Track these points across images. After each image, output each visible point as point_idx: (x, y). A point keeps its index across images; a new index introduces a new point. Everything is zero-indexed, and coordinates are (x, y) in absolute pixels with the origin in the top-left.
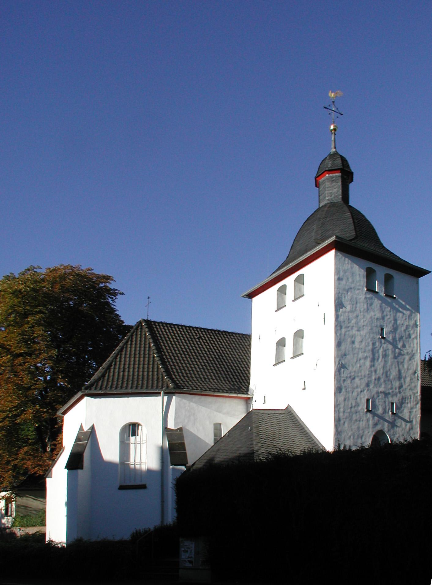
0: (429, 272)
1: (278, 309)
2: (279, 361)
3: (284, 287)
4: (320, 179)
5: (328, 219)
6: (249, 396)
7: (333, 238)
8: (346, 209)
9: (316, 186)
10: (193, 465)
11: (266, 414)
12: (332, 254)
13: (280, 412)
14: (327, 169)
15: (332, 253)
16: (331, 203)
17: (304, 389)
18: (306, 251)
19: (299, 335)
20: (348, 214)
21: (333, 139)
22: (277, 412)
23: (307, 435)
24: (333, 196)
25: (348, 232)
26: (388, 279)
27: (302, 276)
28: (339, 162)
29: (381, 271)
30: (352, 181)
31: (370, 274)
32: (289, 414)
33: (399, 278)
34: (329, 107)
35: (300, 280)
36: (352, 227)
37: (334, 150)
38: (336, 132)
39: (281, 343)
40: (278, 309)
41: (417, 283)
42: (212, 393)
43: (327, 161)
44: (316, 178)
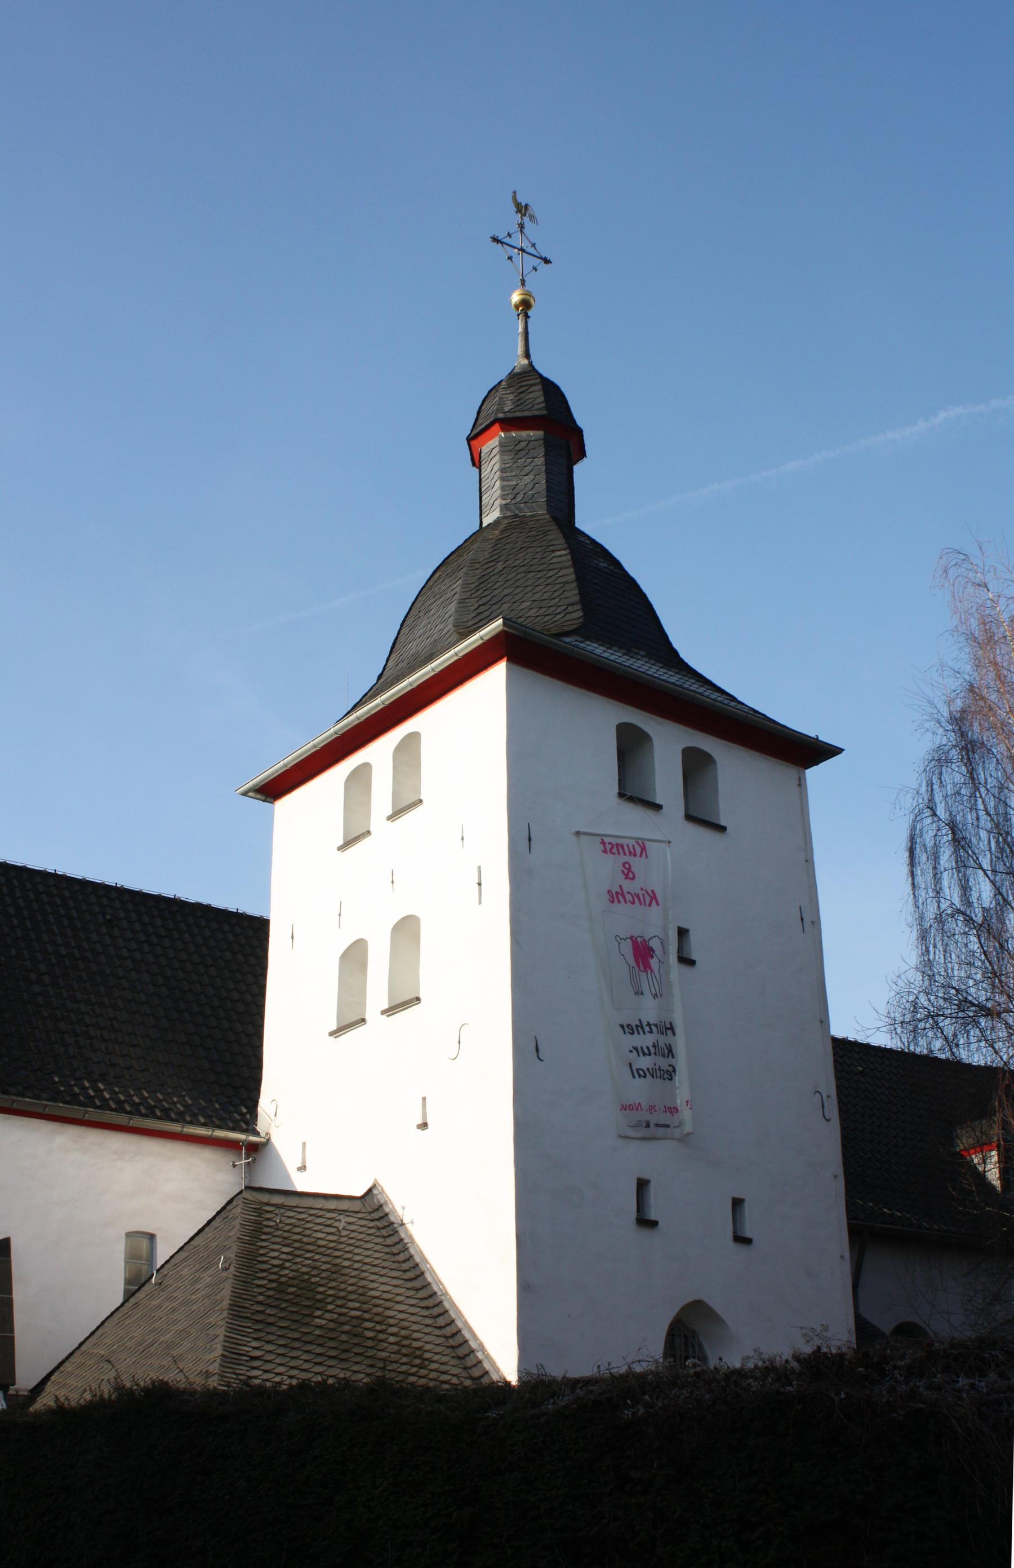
0: (245, 794)
1: (348, 844)
2: (348, 1023)
3: (363, 772)
4: (484, 444)
5: (500, 566)
6: (253, 1139)
7: (496, 625)
8: (556, 537)
9: (474, 464)
10: (39, 1388)
11: (290, 1208)
12: (496, 677)
13: (345, 1205)
14: (501, 416)
15: (498, 673)
16: (516, 516)
17: (424, 1126)
18: (430, 658)
19: (407, 930)
20: (563, 555)
21: (520, 329)
22: (332, 1205)
23: (429, 1303)
24: (519, 498)
25: (553, 603)
26: (696, 765)
27: (414, 738)
28: (537, 395)
29: (668, 743)
30: (582, 454)
31: (631, 745)
32: (372, 1212)
33: (735, 769)
34: (507, 240)
35: (409, 751)
36: (573, 594)
37: (526, 362)
38: (530, 313)
39: (354, 957)
40: (348, 844)
41: (801, 783)
42: (122, 1119)
43: (501, 392)
44: (469, 440)
